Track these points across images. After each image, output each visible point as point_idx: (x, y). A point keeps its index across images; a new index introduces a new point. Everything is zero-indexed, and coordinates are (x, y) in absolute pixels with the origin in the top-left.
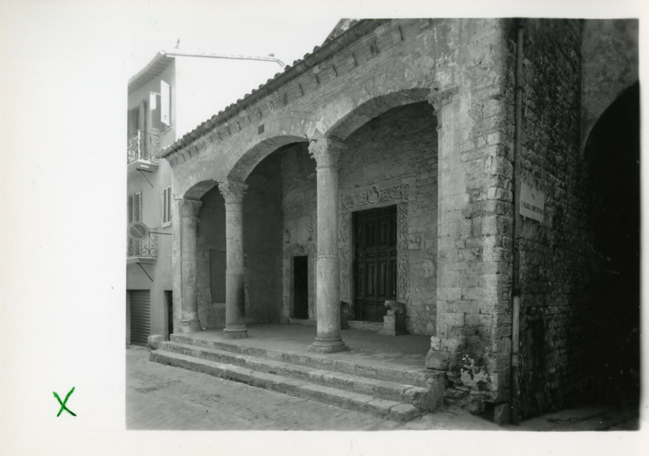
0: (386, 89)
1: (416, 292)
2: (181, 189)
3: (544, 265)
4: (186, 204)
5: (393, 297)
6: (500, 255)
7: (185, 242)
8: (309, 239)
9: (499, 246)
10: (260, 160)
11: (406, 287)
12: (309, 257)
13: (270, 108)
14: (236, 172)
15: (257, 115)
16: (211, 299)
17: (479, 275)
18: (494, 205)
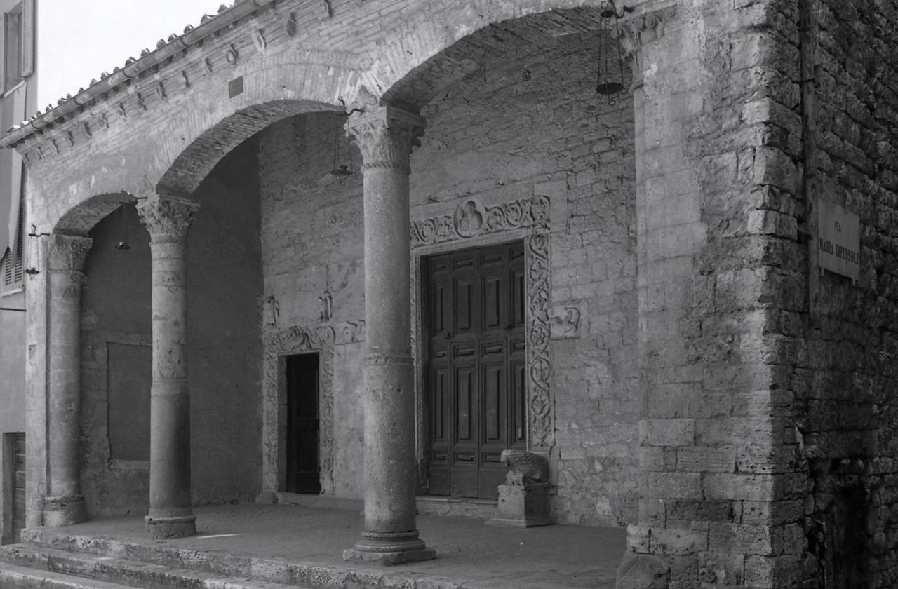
0: (517, 8)
1: (571, 431)
2: (48, 212)
3: (864, 369)
4: (59, 242)
5: (517, 438)
6: (776, 350)
7: (57, 327)
8: (322, 318)
9: (774, 331)
10: (228, 149)
11: (547, 419)
12: (321, 357)
13: (257, 43)
14: (176, 175)
15: (227, 57)
16: (108, 450)
17: (733, 391)
18: (762, 246)
